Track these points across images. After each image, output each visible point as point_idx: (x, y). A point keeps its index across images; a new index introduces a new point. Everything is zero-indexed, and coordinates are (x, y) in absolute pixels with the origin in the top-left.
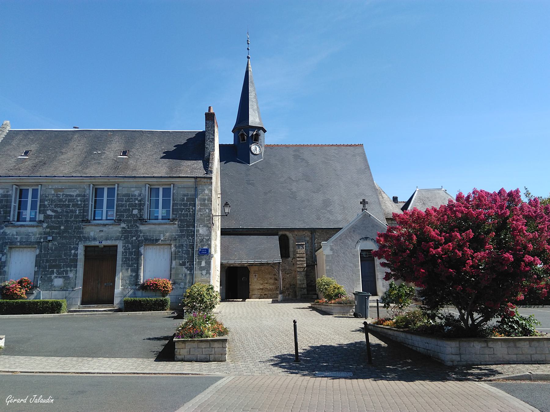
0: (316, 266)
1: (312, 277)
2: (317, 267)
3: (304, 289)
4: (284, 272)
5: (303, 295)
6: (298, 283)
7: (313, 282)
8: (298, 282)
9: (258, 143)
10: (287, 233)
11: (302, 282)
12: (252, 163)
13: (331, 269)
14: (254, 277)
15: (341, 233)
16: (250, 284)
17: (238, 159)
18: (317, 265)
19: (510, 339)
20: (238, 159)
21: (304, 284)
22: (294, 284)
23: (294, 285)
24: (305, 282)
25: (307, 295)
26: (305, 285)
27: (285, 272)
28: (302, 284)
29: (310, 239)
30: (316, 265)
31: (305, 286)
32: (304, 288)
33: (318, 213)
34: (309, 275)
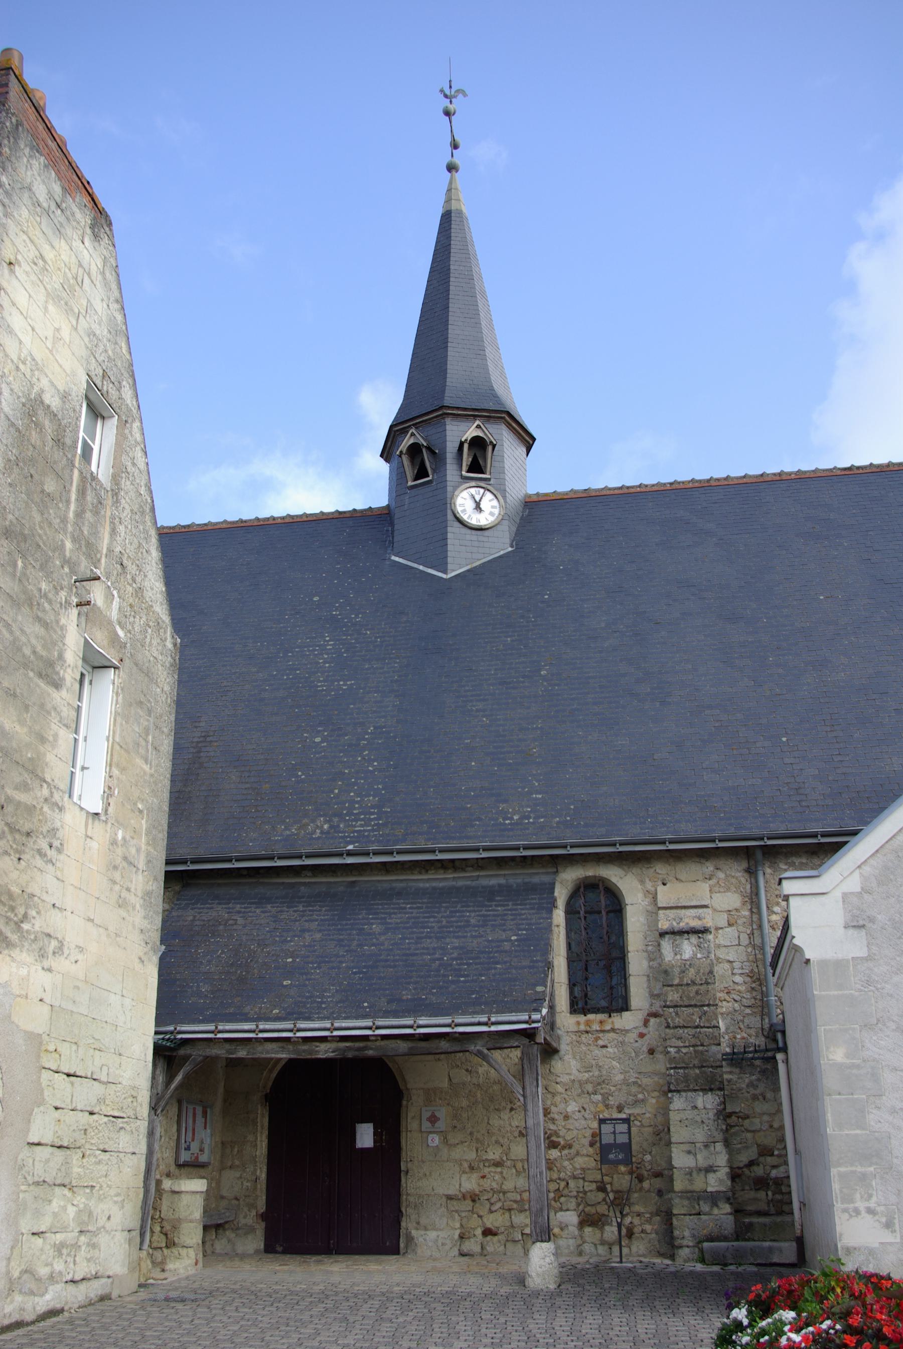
0: (780, 1057)
1: (765, 1126)
2: (786, 1061)
3: (715, 1204)
4: (599, 1097)
5: (711, 1239)
6: (676, 1162)
7: (772, 1155)
8: (681, 1160)
9: (489, 479)
10: (613, 874)
11: (699, 1157)
12: (453, 570)
13: (858, 1067)
14: (426, 1125)
15: (562, 948)
16: (403, 1168)
17: (397, 559)
18: (785, 1049)
19: (457, 1035)
20: (397, 559)
21: (710, 1169)
22: (657, 1169)
23: (658, 1175)
24: (721, 1159)
25: (737, 1240)
26: (723, 1173)
27: (606, 1097)
28: (700, 1170)
29: (744, 903)
30: (779, 1050)
31: (717, 1182)
32: (714, 1199)
33: (787, 761)
34: (747, 1117)
